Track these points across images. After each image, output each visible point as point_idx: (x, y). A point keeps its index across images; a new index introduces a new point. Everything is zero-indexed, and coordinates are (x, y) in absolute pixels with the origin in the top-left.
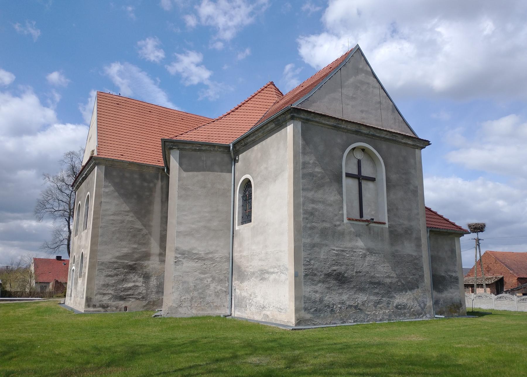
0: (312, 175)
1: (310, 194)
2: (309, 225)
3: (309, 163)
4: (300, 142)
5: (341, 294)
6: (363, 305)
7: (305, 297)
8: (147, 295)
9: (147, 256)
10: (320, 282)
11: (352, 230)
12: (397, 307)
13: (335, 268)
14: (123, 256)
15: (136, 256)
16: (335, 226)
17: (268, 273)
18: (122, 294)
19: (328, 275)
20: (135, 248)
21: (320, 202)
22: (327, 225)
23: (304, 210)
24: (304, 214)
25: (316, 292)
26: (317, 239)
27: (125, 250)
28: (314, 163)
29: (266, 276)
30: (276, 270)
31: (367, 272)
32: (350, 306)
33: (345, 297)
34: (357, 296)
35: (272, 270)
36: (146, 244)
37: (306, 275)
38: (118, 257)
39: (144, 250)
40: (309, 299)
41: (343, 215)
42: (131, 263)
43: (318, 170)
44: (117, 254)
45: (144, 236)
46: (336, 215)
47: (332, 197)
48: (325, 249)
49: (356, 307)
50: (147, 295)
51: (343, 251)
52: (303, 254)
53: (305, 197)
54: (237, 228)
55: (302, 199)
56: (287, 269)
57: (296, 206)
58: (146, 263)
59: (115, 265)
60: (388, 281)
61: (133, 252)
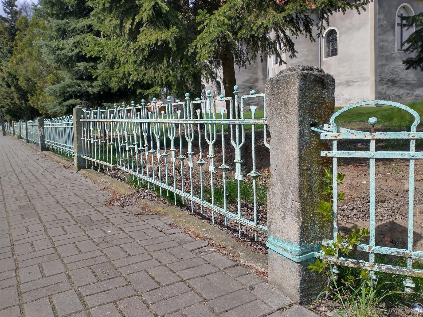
0: (382, 26)
1: (381, 37)
2: (381, 55)
3: (381, 19)
4: (377, 7)
5: (393, 90)
6: (402, 95)
7: (379, 92)
8: (259, 102)
9: (257, 80)
10: (385, 84)
11: (399, 55)
12: (416, 96)
13: (391, 76)
14: (246, 81)
15: (252, 81)
16: (392, 54)
17: (353, 82)
18: (248, 102)
19: (388, 80)
20: (251, 76)
21: (385, 41)
22: (388, 54)
23: (379, 46)
24: (379, 48)
25: (383, 89)
26: (384, 62)
27: (247, 78)
28: (383, 19)
29: (351, 83)
30: (360, 80)
31: (404, 78)
32: (397, 96)
33: (395, 91)
34: (399, 90)
35: (357, 80)
36: (256, 73)
37: (380, 81)
38: (244, 82)
39: (255, 77)
40: (380, 92)
41: (395, 47)
42: (250, 85)
43: (385, 22)
44: (243, 80)
45: (254, 68)
46: (392, 48)
47: (391, 38)
48: (388, 67)
49: (399, 96)
50: (259, 102)
51: (395, 67)
52: (378, 70)
53: (379, 39)
54: (324, 59)
55: (378, 40)
56: (369, 79)
57: (376, 44)
58: (257, 84)
59: (243, 87)
60: (413, 82)
61: (251, 79)
